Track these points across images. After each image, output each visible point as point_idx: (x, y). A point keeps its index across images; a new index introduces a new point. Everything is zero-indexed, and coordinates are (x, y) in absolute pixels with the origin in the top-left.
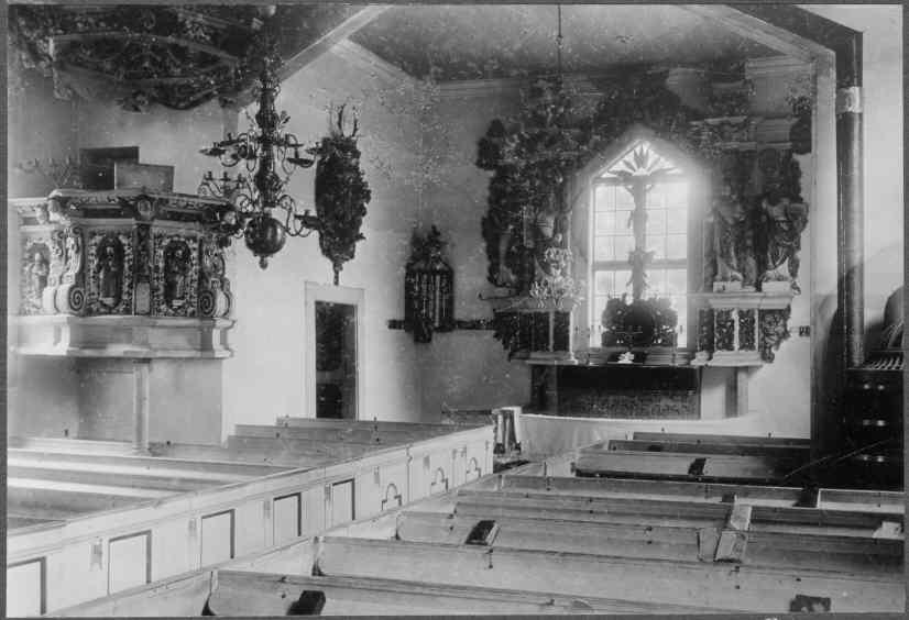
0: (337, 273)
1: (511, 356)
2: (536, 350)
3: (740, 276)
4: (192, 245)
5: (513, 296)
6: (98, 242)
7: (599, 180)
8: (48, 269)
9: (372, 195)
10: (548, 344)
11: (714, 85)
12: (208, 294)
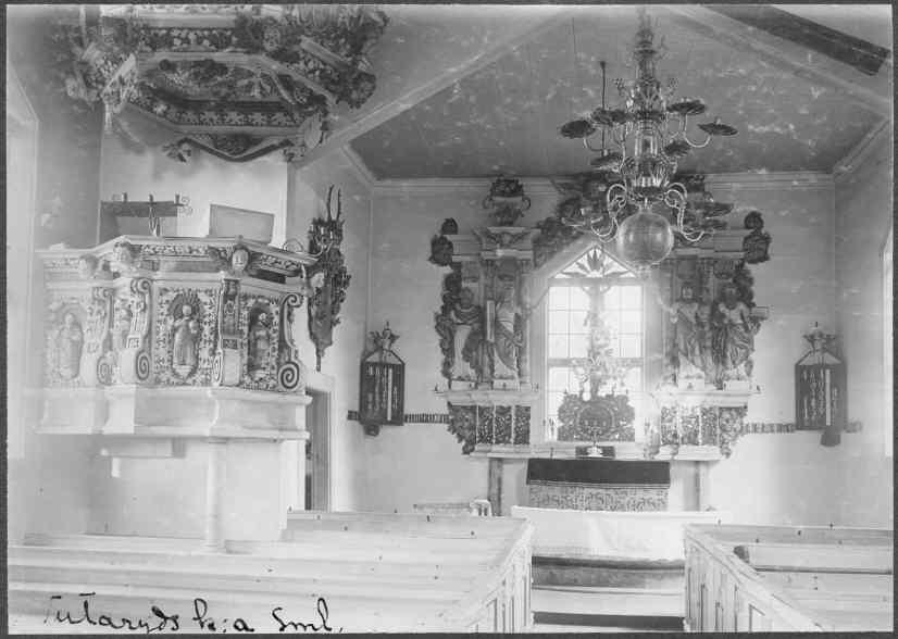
0: (319, 357)
1: (466, 452)
2: (498, 442)
3: (703, 374)
4: (274, 308)
5: (472, 390)
6: (170, 299)
7: (553, 282)
8: (82, 334)
9: (351, 281)
10: (510, 437)
11: (494, 198)
12: (292, 366)
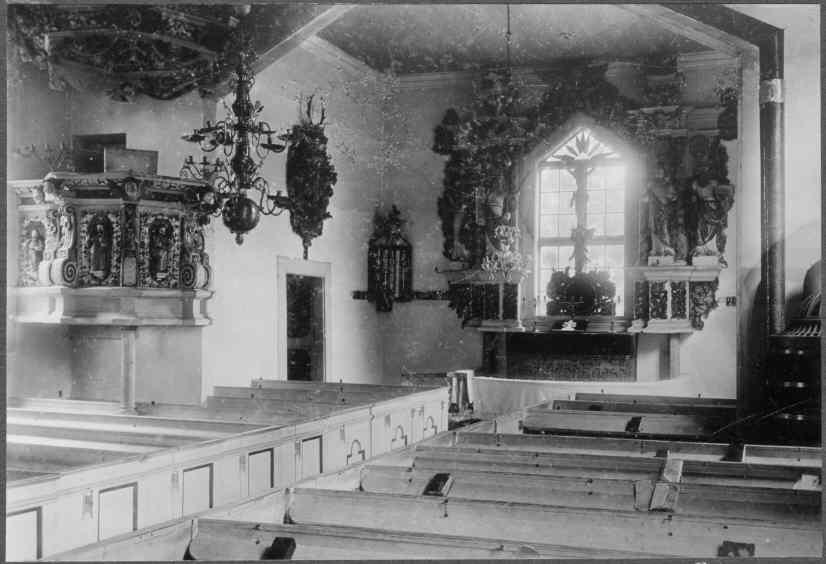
1: (464, 324)
2: (487, 318)
6: (89, 220)
7: (544, 164)
8: (44, 245)
10: (498, 313)
12: (189, 268)
